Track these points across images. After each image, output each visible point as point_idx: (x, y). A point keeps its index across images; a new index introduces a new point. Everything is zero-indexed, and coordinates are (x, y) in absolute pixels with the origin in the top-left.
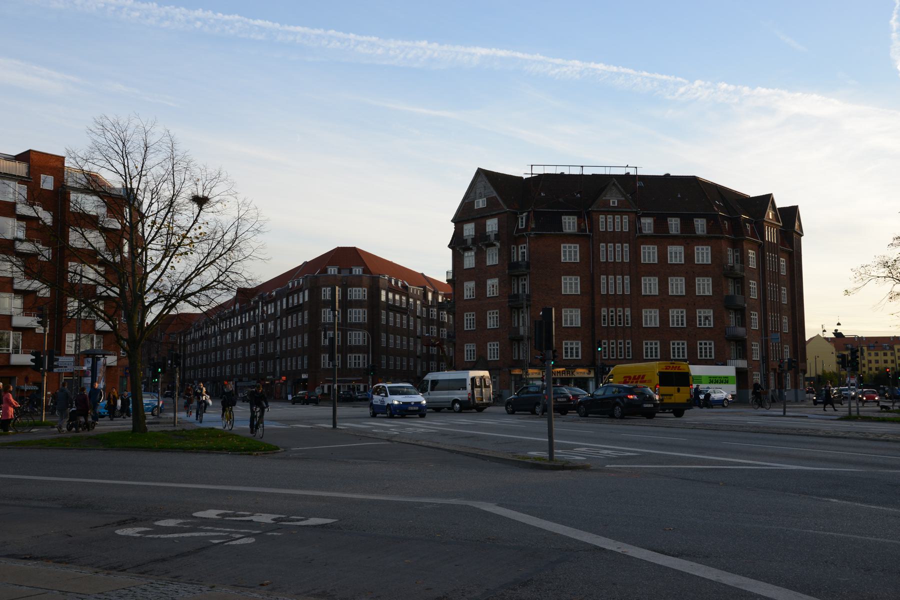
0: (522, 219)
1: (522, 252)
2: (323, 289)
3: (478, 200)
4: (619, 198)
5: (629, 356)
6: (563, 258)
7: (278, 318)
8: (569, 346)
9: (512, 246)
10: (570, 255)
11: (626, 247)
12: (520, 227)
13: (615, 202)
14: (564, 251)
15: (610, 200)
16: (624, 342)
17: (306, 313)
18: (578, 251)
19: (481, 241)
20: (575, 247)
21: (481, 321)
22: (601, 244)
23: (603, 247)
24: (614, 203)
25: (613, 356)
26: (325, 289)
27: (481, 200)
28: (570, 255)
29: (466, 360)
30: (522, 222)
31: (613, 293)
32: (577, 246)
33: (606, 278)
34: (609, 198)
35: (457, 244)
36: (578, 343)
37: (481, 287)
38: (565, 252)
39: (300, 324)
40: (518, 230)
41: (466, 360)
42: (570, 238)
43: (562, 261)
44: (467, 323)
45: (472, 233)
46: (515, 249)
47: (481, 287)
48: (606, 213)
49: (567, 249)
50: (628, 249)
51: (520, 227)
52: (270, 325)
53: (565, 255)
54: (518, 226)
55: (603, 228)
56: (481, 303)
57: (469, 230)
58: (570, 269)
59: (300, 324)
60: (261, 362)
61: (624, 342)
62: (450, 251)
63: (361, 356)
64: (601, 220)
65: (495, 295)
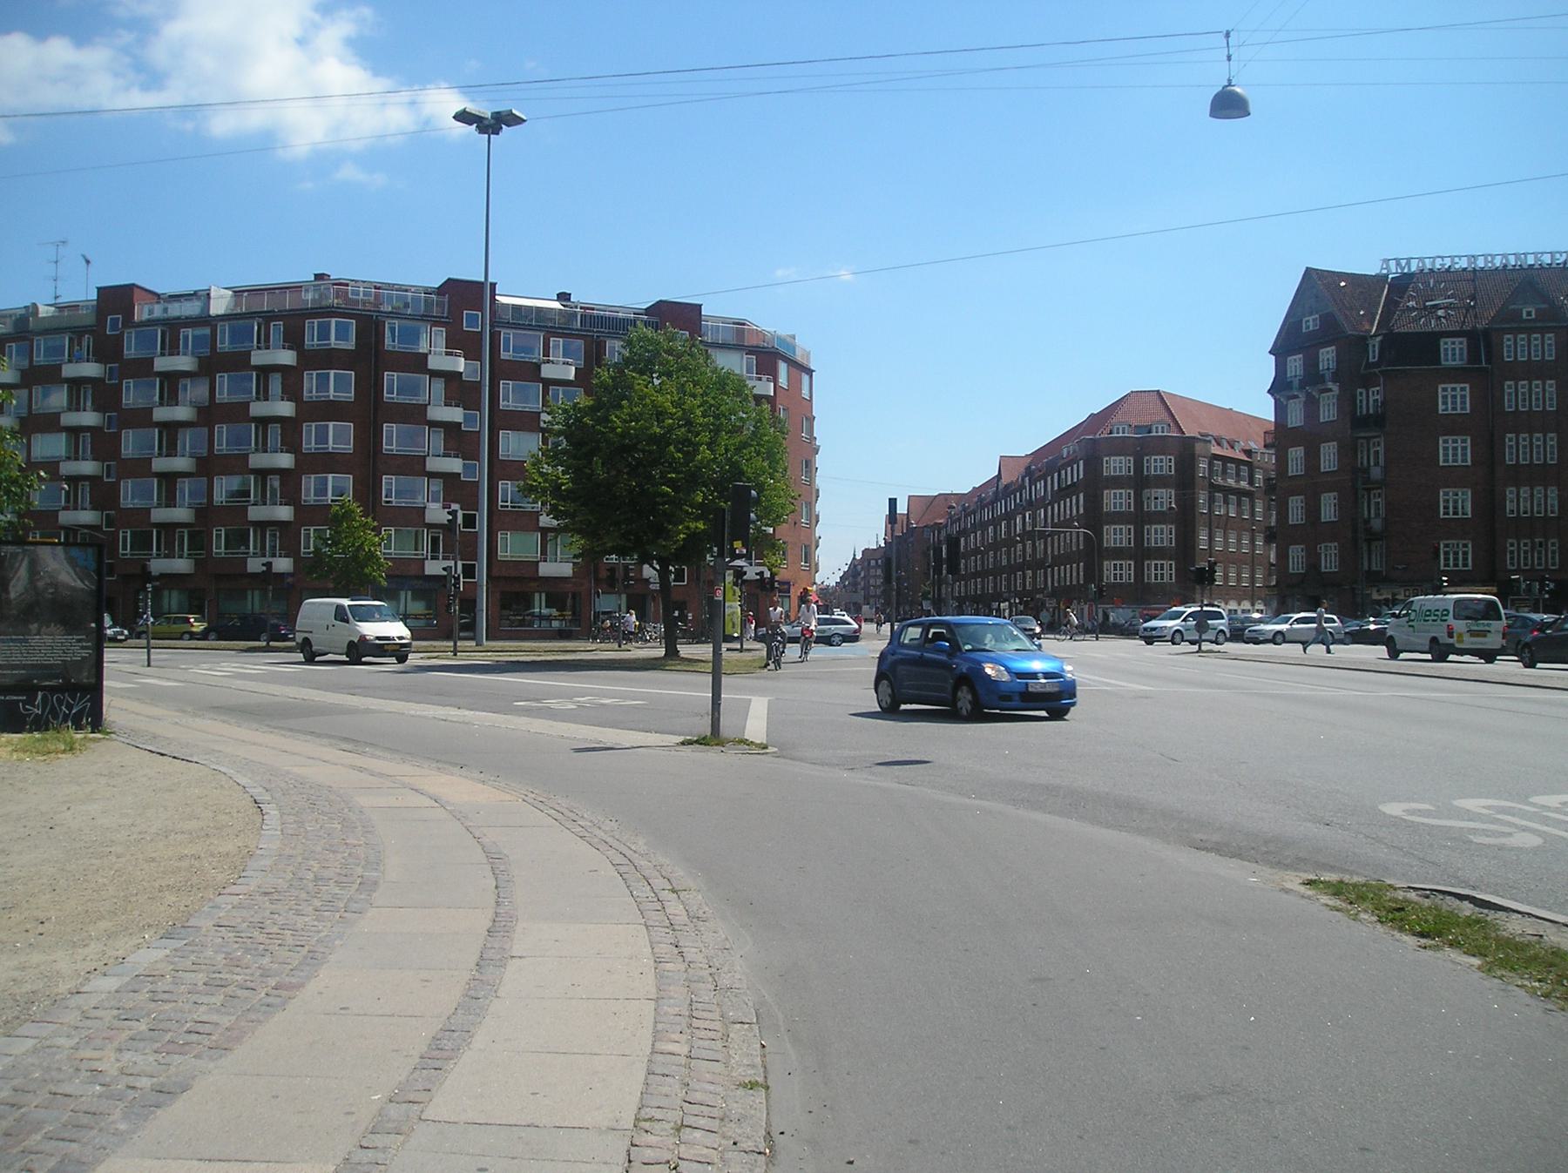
0: (1374, 346)
1: (1374, 400)
2: (1105, 459)
3: (1307, 319)
4: (1538, 306)
5: (1553, 564)
6: (1441, 407)
7: (1049, 567)
8: (1450, 346)
9: (1359, 390)
10: (1454, 403)
11: (1551, 386)
12: (1371, 360)
13: (1531, 312)
14: (1444, 447)
15: (1521, 310)
16: (1545, 436)
17: (1081, 496)
18: (1468, 396)
19: (1312, 377)
20: (1464, 441)
21: (1313, 510)
22: (1509, 435)
23: (1510, 387)
24: (1529, 314)
25: (1526, 565)
26: (1108, 458)
27: (1311, 318)
28: (1454, 403)
29: (1291, 571)
30: (1374, 351)
31: (1525, 359)
32: (1466, 387)
33: (1514, 438)
34: (1520, 307)
35: (1279, 388)
36: (1466, 440)
37: (1312, 457)
38: (1445, 397)
39: (1074, 583)
40: (1369, 365)
41: (1291, 571)
42: (1454, 375)
43: (1440, 412)
44: (1292, 466)
45: (1300, 372)
46: (1364, 395)
47: (1312, 457)
48: (1515, 331)
49: (1449, 393)
50: (1553, 389)
51: (1371, 360)
52: (1040, 545)
53: (1445, 403)
54: (1368, 359)
55: (1510, 407)
56: (1312, 484)
57: (1295, 364)
58: (1454, 425)
59: (1074, 583)
60: (1029, 573)
61: (1545, 436)
62: (1273, 357)
63: (1153, 581)
64: (1507, 391)
65: (1331, 419)
